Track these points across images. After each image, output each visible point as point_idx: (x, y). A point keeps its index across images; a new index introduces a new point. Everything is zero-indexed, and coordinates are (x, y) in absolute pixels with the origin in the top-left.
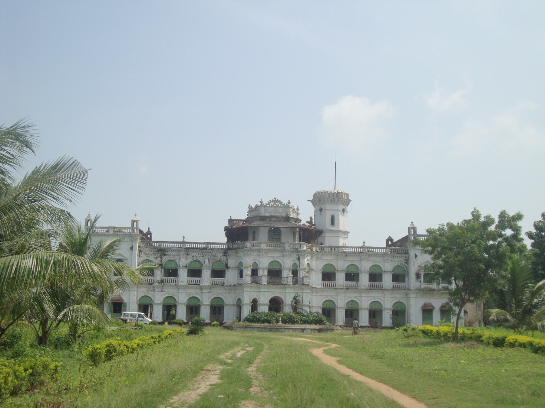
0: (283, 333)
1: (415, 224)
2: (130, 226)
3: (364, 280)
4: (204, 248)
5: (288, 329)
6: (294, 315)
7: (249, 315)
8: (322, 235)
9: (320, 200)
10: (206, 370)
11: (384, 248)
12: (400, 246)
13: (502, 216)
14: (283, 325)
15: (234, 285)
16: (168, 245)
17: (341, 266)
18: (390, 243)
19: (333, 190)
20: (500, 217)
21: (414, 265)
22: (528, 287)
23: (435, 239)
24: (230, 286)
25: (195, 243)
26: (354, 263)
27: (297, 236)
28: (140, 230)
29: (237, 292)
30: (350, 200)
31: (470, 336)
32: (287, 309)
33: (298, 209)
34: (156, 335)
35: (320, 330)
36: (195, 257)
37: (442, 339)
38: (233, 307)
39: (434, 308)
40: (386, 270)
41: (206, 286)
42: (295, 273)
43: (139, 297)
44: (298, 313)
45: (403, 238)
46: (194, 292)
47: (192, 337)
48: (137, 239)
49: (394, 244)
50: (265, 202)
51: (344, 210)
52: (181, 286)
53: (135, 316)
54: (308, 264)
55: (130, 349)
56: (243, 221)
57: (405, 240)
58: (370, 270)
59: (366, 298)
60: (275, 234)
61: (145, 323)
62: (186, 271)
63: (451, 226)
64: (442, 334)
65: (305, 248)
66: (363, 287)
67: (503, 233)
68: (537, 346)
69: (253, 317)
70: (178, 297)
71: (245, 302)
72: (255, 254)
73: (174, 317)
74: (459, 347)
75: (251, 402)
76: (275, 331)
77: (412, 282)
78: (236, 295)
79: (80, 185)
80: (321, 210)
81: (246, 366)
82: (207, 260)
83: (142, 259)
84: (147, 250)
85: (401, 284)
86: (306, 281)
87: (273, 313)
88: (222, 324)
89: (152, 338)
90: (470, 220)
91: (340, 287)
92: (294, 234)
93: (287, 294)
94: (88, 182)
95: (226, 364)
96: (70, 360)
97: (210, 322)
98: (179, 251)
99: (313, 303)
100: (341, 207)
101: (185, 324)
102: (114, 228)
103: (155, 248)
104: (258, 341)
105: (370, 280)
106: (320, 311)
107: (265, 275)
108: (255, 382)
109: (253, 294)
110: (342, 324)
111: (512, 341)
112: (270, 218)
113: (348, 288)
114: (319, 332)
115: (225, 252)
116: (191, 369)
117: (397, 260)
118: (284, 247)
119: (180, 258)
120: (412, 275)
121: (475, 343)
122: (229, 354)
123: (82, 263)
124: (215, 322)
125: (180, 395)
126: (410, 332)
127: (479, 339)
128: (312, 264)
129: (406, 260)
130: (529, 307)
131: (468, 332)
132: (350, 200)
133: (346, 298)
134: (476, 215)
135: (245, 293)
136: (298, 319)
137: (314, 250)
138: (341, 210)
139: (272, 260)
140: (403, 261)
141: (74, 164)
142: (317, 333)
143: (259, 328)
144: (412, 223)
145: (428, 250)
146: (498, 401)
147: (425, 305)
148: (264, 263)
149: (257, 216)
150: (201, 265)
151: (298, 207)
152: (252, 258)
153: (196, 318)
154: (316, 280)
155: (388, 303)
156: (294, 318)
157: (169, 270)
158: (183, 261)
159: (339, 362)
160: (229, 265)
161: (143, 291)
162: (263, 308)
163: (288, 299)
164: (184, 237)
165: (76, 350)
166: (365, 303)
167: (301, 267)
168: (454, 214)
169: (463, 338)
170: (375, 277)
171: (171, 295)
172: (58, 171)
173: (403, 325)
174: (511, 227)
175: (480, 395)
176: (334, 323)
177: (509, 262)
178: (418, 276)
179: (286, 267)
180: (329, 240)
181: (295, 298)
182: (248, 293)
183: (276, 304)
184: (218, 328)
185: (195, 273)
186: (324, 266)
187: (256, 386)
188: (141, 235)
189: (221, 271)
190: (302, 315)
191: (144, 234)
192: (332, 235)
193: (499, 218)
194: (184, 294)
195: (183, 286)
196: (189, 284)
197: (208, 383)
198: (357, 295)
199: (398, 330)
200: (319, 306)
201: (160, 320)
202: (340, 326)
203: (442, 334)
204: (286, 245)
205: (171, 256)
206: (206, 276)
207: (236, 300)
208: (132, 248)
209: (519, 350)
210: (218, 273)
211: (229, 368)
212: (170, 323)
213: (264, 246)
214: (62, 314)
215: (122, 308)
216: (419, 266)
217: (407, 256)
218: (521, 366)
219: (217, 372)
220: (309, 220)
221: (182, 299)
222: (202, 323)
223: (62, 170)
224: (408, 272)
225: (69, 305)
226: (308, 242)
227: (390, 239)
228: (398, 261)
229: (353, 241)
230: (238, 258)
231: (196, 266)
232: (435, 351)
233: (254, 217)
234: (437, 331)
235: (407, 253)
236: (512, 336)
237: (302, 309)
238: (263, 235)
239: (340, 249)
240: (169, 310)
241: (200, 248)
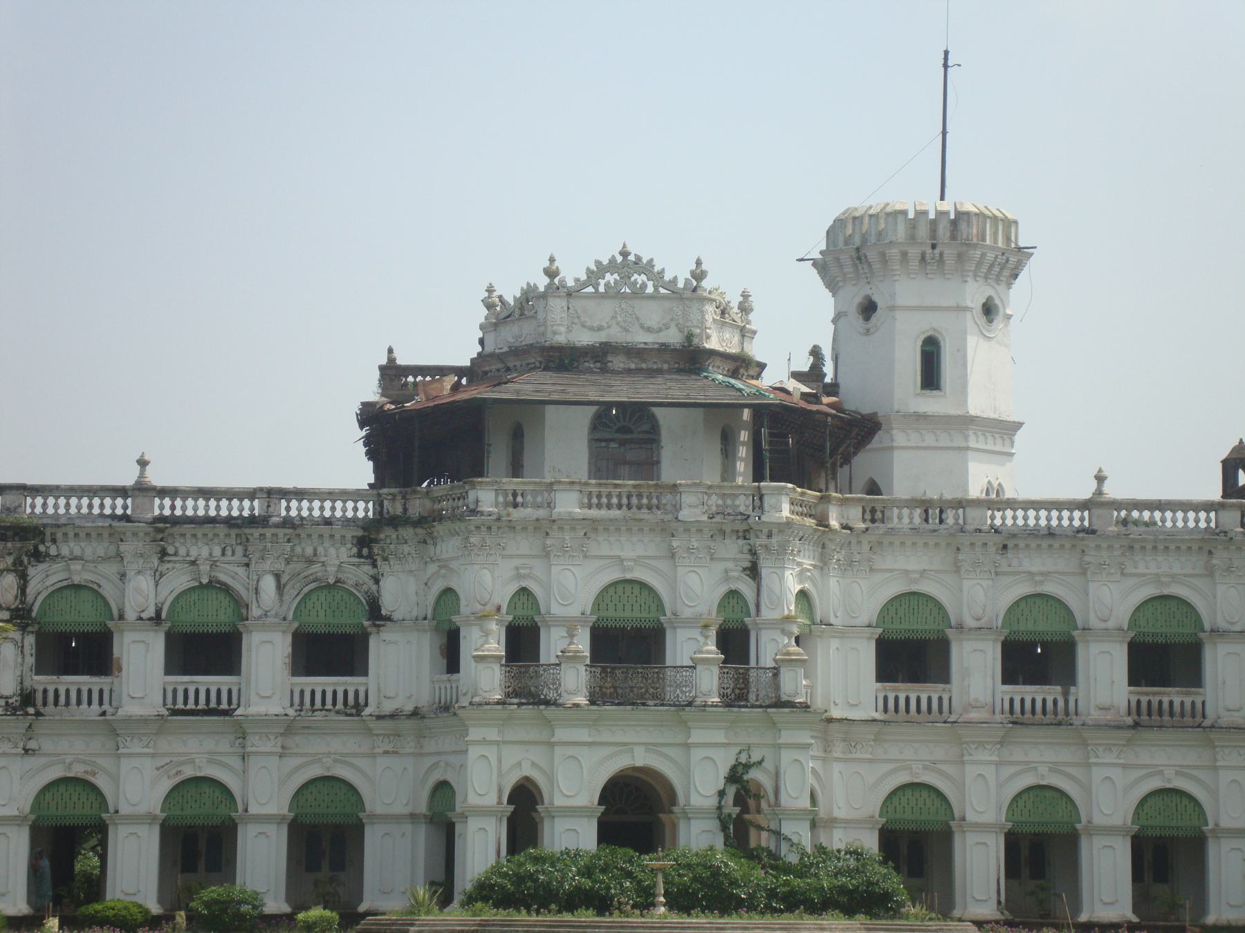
9: (857, 256)
26: (1050, 588)
51: (989, 310)
80: (868, 309)
92: (727, 441)
100: (974, 293)
109: (512, 755)
115: (367, 539)
128: (822, 592)
148: (572, 591)
160: (388, 604)
162: (572, 834)
180: (909, 469)
183: (635, 810)
238: (565, 446)
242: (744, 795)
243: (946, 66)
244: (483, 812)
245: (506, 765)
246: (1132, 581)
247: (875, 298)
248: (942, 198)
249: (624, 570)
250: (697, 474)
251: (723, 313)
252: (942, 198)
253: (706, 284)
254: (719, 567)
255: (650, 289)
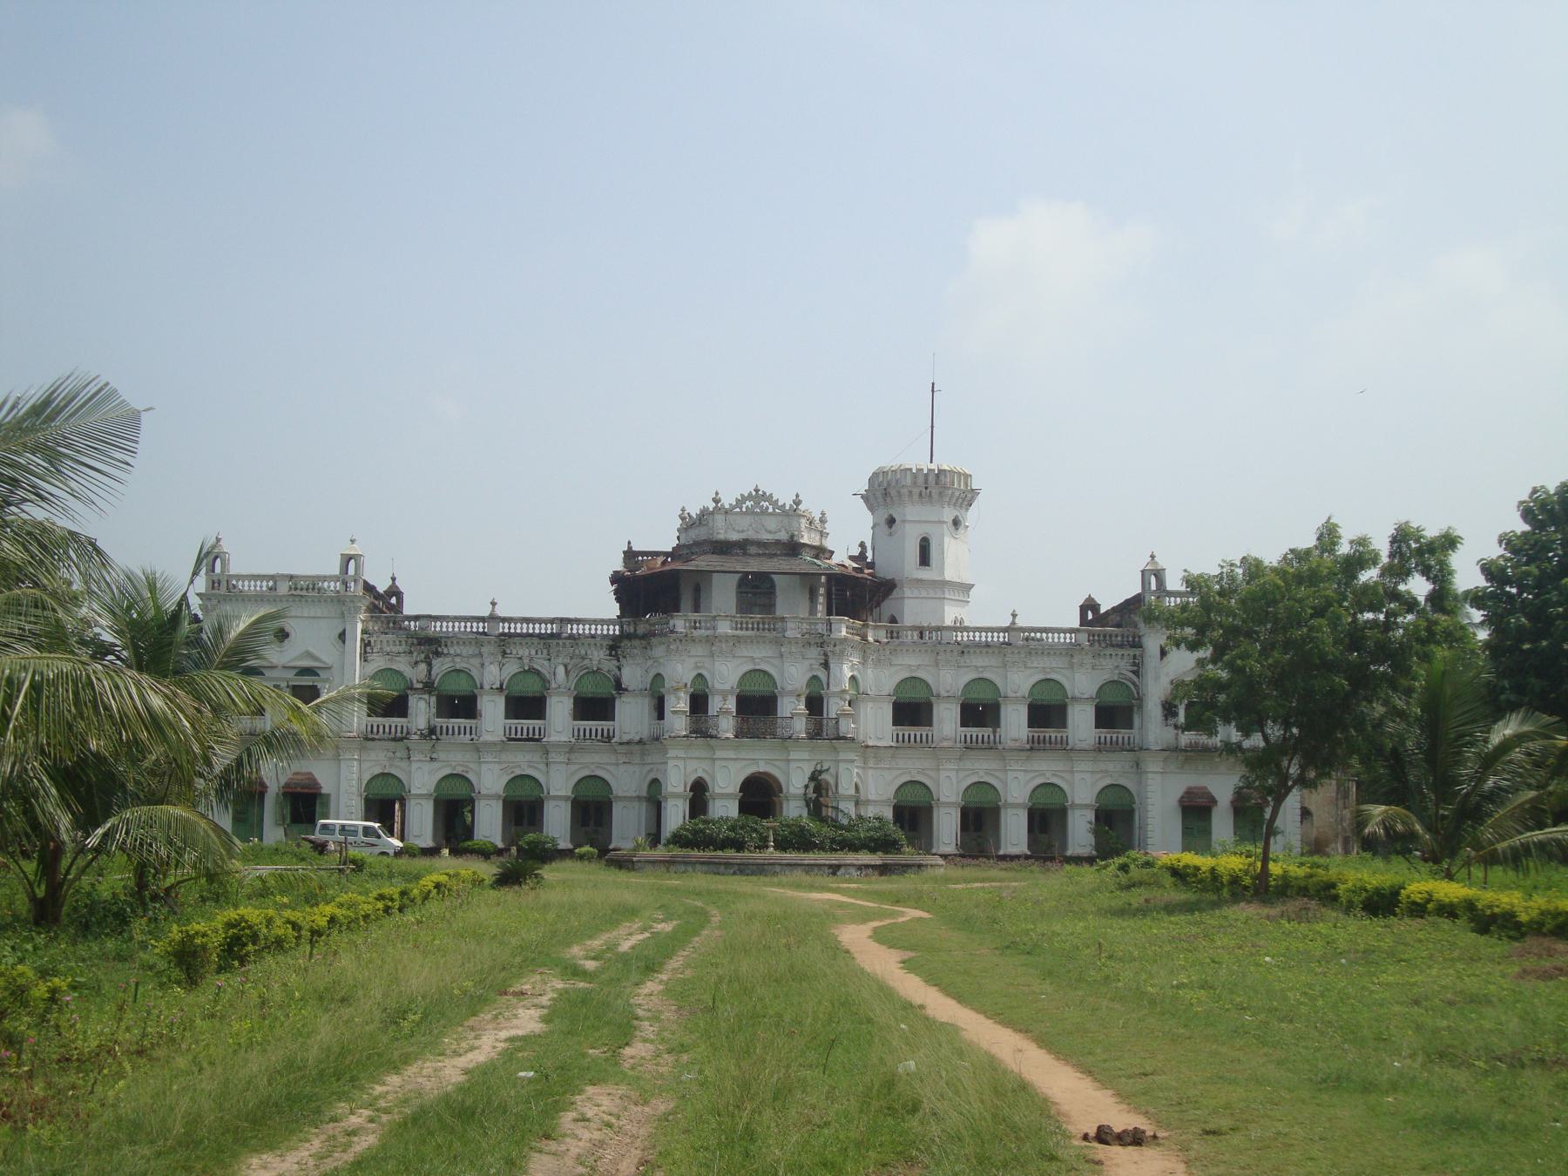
0: (775, 880)
1: (1162, 562)
2: (336, 571)
3: (1015, 723)
4: (552, 636)
5: (792, 866)
6: (812, 826)
7: (683, 828)
8: (895, 593)
9: (885, 492)
10: (515, 994)
11: (1071, 631)
12: (1118, 626)
13: (1401, 537)
14: (778, 854)
15: (640, 742)
16: (447, 627)
17: (949, 682)
18: (1090, 616)
19: (925, 465)
20: (1394, 540)
21: (1157, 678)
22: (1471, 744)
23: (1206, 606)
24: (628, 743)
25: (527, 620)
26: (987, 675)
27: (821, 599)
28: (365, 582)
29: (649, 759)
30: (974, 493)
31: (1303, 884)
32: (793, 810)
33: (823, 521)
34: (392, 890)
35: (884, 870)
36: (526, 661)
37: (1225, 893)
38: (636, 804)
39: (1214, 801)
40: (1077, 694)
41: (558, 745)
42: (815, 704)
43: (367, 777)
44: (823, 820)
45: (1127, 602)
46: (524, 761)
47: (508, 894)
48: (357, 610)
49: (1101, 619)
50: (728, 500)
51: (956, 523)
52: (486, 744)
53: (354, 833)
54: (853, 678)
55: (303, 933)
56: (666, 554)
57: (1131, 607)
58: (1031, 693)
59: (1021, 776)
60: (757, 593)
61: (383, 853)
62: (500, 703)
63: (1254, 568)
64: (1225, 879)
65: (844, 633)
66: (1010, 744)
67: (1402, 587)
68: (1488, 912)
69: (695, 832)
70: (479, 775)
71: (670, 789)
72: (699, 650)
73: (469, 832)
74: (1268, 917)
75: (611, 1089)
76: (753, 873)
77: (1153, 728)
78: (648, 768)
79: (118, 455)
80: (891, 522)
81: (635, 977)
82: (561, 670)
83: (373, 667)
84: (389, 642)
85: (1122, 734)
86: (847, 727)
87: (752, 820)
88: (604, 851)
89: (381, 897)
90: (1308, 552)
91: (945, 744)
93: (793, 765)
94: (141, 448)
95: (576, 972)
96: (120, 965)
97: (570, 846)
98: (480, 644)
99: (868, 789)
100: (948, 514)
101: (500, 852)
102: (291, 577)
103: (411, 635)
104: (699, 904)
105: (1032, 723)
106: (888, 814)
107: (727, 712)
108: (648, 1029)
110: (950, 849)
111: (1417, 898)
112: (742, 547)
113: (970, 746)
114: (881, 874)
115: (615, 646)
116: (465, 993)
117: (1109, 664)
118: (784, 630)
119: (483, 665)
120: (1153, 708)
121: (1313, 904)
122: (597, 943)
123: (117, 687)
124: (586, 849)
125: (411, 1070)
126: (1135, 873)
127: (1326, 894)
128: (863, 676)
129: (1134, 664)
130: (1474, 799)
131: (1297, 871)
132: (974, 493)
133: (962, 774)
134: (1328, 536)
135: (671, 763)
136: (824, 836)
137: (870, 639)
138: (950, 521)
139: (750, 667)
140: (1125, 666)
141: (104, 395)
142: (875, 877)
143: (709, 863)
144: (1153, 557)
145: (1184, 639)
146: (1324, 1081)
147: (1189, 793)
148: (726, 675)
149: (704, 542)
150: (545, 682)
151: (823, 514)
152: (690, 663)
153: (531, 836)
154: (875, 724)
155: (1083, 788)
156: (813, 835)
157: (452, 698)
158: (493, 673)
159: (908, 965)
160: (625, 682)
161: (377, 761)
162: (725, 808)
163: (795, 781)
164: (493, 604)
165: (138, 937)
166: (1017, 787)
167: (833, 689)
168: (1262, 529)
169: (1285, 890)
170: (1047, 713)
171: (459, 770)
172: (51, 418)
173: (1118, 853)
174: (1426, 572)
175: (1280, 1063)
176: (928, 848)
177: (1421, 671)
178: (1169, 710)
179: (789, 688)
180: (913, 610)
181: (814, 777)
182: (681, 763)
183: (759, 795)
184: (593, 866)
185: (526, 705)
187: (645, 1041)
188: (369, 599)
190: (837, 826)
191: (378, 596)
192: (924, 594)
193: (1392, 543)
194: (497, 767)
195: (494, 744)
196: (510, 740)
197: (504, 1034)
198: (994, 765)
199: (1105, 867)
200: (884, 797)
201: (427, 841)
202: (944, 856)
203: (1225, 879)
204: (790, 625)
205: (458, 659)
206: (560, 715)
208: (342, 636)
209: (1434, 924)
210: (594, 707)
211: (582, 985)
212: (455, 852)
213: (724, 628)
214: (100, 831)
215: (318, 809)
217: (1137, 652)
218: (1434, 972)
219: (545, 1000)
220: (856, 552)
221: (491, 780)
222: (545, 850)
223: (65, 414)
224: (1140, 699)
225: (123, 806)
226: (854, 615)
227: (1089, 606)
228: (1113, 666)
229: (982, 611)
230: (650, 663)
231: (531, 687)
232: (1194, 930)
233: (697, 544)
234: (1213, 869)
235: (1137, 644)
236: (1420, 884)
237: (836, 808)
238: (723, 595)
239: (946, 634)
240: (454, 816)
241: (540, 636)
250: (793, 609)
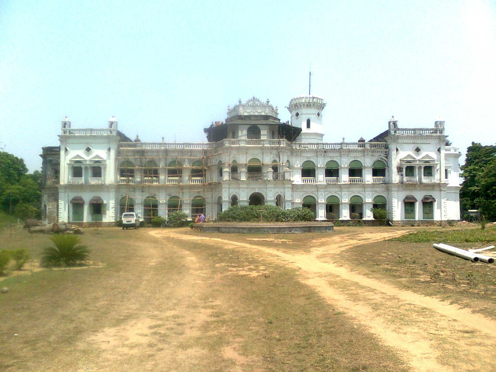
1: (241, 100)
26: (335, 159)
42: (275, 169)
93: (268, 190)
109: (277, 190)
112: (249, 117)
117: (377, 154)
129: (386, 154)
135: (223, 190)
140: (383, 156)
147: (407, 198)
148: (243, 160)
163: (270, 196)
178: (400, 169)
183: (256, 199)
186: (303, 164)
189: (385, 174)
206: (345, 177)
207: (217, 198)
216: (400, 160)
217: (387, 150)
235: (387, 147)
238: (243, 134)
242: (279, 200)
243: (310, 74)
244: (225, 201)
245: (230, 192)
246: (350, 158)
247: (299, 113)
248: (310, 94)
249: (254, 156)
251: (272, 109)
252: (310, 94)
253: (270, 103)
254: (272, 156)
255: (259, 105)
